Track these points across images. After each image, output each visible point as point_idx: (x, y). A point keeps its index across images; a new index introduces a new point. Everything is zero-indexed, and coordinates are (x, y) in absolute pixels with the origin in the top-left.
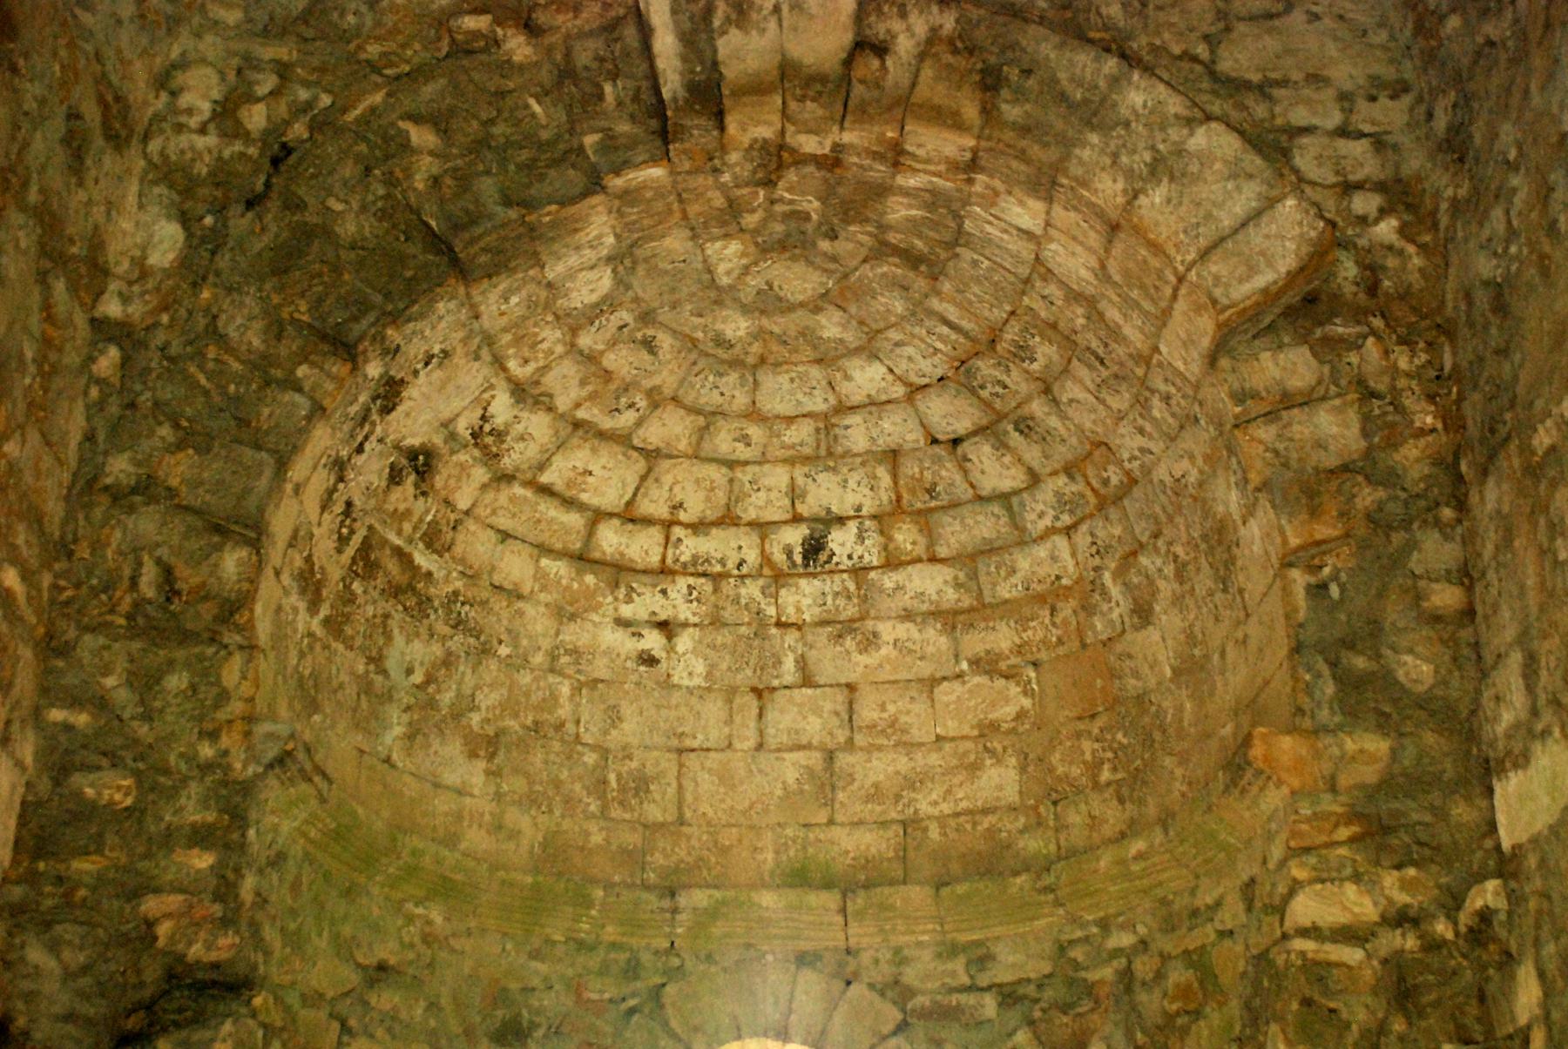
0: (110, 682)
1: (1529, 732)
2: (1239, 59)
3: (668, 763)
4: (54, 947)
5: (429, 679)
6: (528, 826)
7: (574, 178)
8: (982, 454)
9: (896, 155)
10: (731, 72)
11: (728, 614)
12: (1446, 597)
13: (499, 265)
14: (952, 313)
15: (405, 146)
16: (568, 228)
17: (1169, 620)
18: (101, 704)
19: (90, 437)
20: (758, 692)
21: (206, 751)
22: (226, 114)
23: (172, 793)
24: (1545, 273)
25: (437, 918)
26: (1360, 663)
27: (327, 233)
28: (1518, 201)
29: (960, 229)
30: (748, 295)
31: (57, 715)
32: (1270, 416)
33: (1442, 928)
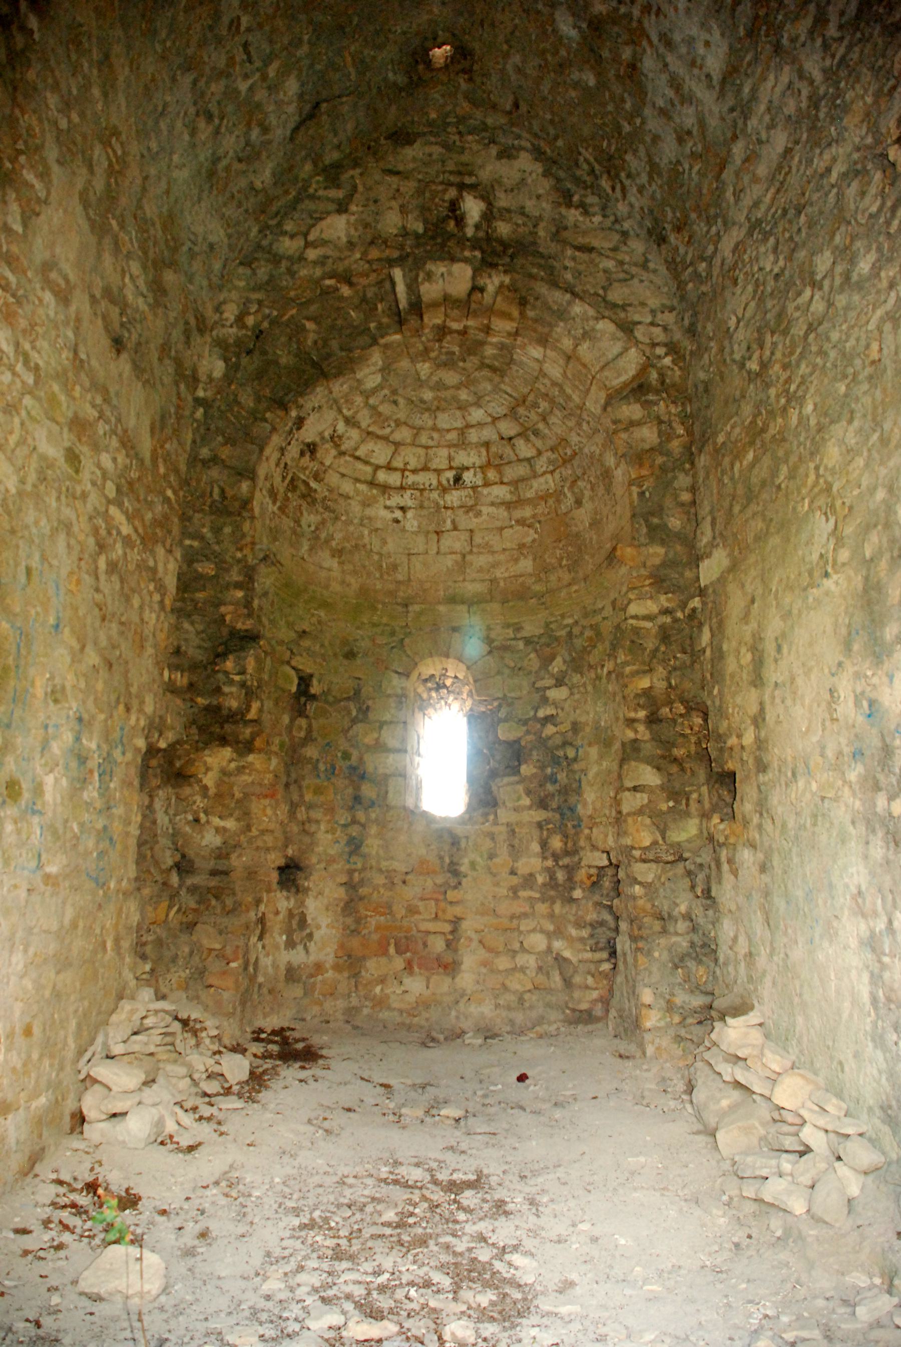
0: (205, 530)
1: (712, 545)
2: (616, 295)
3: (405, 559)
4: (192, 623)
5: (317, 529)
6: (355, 583)
7: (367, 339)
8: (520, 443)
9: (487, 330)
10: (425, 299)
11: (426, 504)
12: (686, 497)
13: (339, 374)
14: (509, 390)
15: (303, 329)
16: (363, 359)
17: (588, 505)
18: (202, 538)
19: (194, 442)
20: (437, 533)
21: (239, 555)
22: (240, 320)
23: (227, 570)
24: (722, 378)
25: (322, 614)
26: (656, 521)
27: (276, 363)
28: (714, 351)
29: (512, 359)
30: (431, 384)
31: (188, 542)
32: (626, 429)
33: (679, 615)
